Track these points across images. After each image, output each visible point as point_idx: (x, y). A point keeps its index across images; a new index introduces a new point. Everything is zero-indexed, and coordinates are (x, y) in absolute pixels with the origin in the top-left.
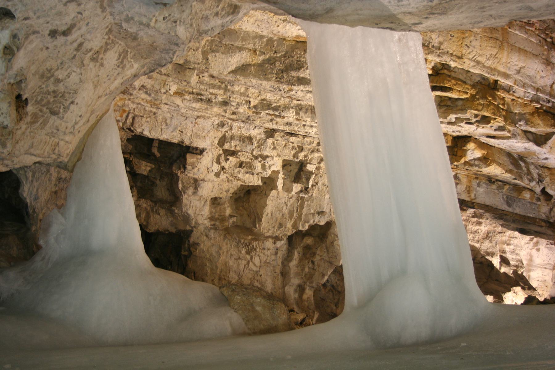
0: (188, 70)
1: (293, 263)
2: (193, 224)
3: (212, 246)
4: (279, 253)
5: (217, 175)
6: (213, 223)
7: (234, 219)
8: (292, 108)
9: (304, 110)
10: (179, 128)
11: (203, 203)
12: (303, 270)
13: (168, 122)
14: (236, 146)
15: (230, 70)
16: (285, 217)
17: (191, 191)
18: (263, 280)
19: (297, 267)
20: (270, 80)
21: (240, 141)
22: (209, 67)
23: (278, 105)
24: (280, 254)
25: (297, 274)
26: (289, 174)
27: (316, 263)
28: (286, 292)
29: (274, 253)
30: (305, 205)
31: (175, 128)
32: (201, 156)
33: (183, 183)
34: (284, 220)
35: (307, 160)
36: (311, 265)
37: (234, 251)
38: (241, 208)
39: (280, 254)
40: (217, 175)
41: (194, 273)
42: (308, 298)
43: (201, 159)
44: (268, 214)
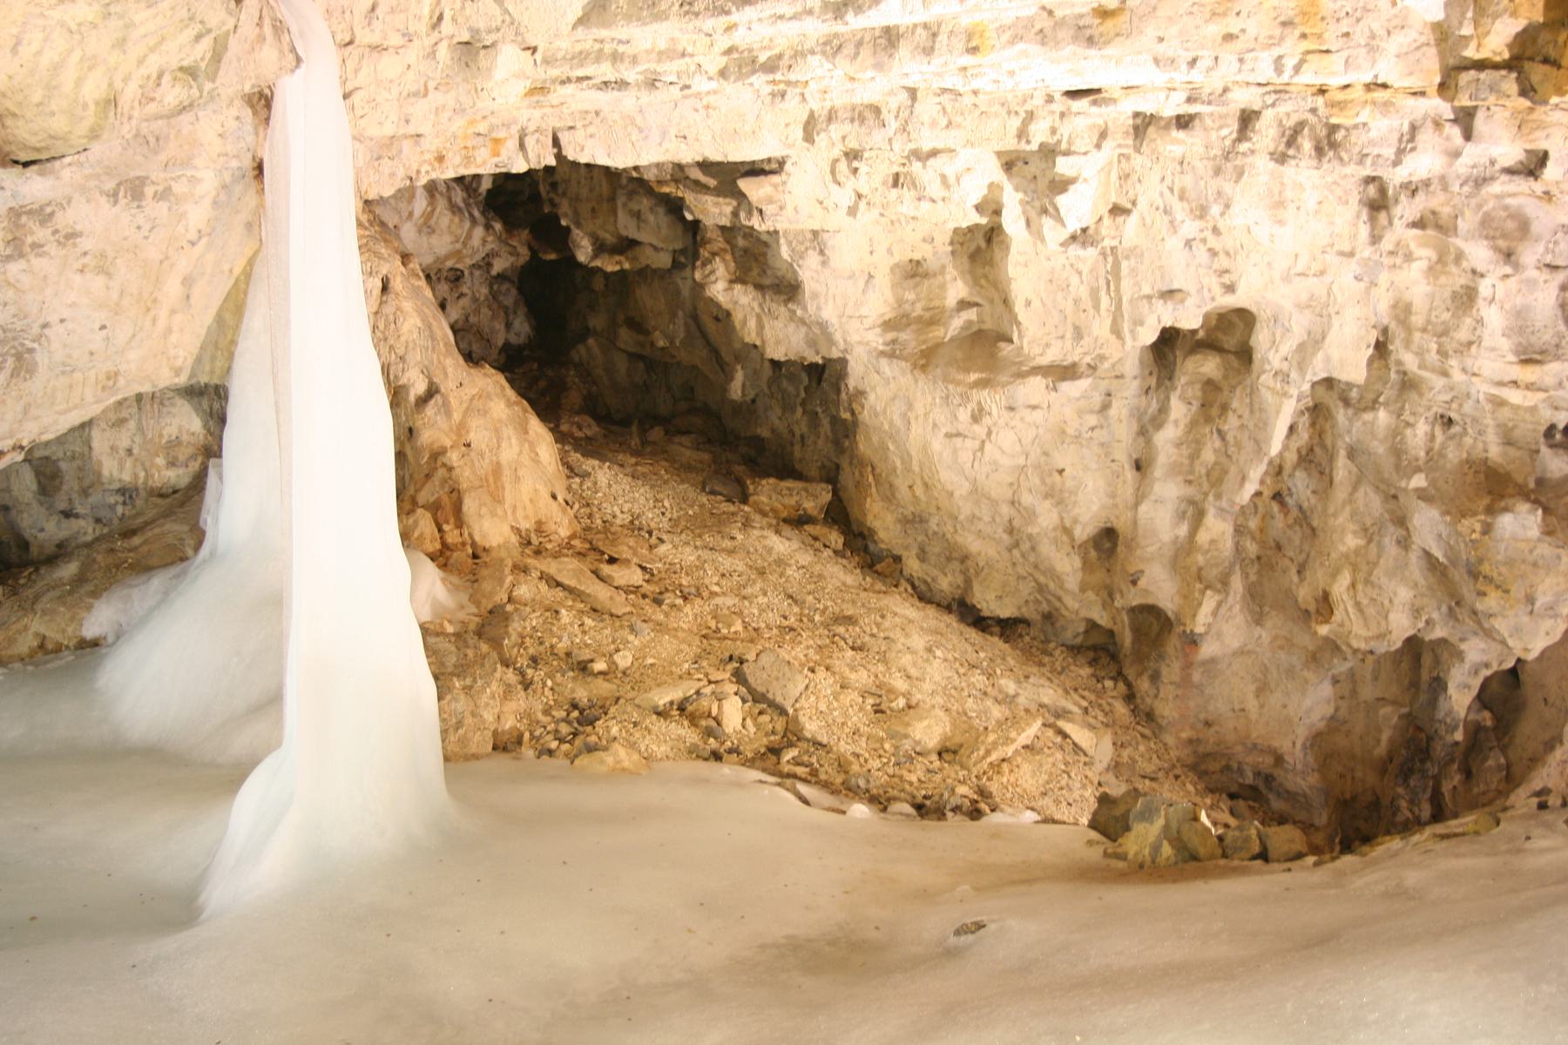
0: (482, 52)
1: (1166, 438)
2: (842, 345)
3: (893, 399)
4: (1115, 404)
5: (852, 211)
6: (891, 336)
7: (972, 314)
8: (813, 52)
9: (849, 49)
10: (673, 132)
11: (861, 283)
12: (1195, 456)
13: (639, 121)
14: (844, 138)
15: (572, 17)
16: (1082, 307)
17: (813, 260)
18: (1070, 484)
19: (1178, 445)
20: (667, 18)
21: (852, 121)
22: (522, 30)
23: (776, 51)
24: (1119, 409)
25: (1174, 469)
26: (1032, 186)
27: (1230, 437)
28: (1141, 522)
29: (1097, 407)
30: (1125, 271)
31: (664, 134)
32: (784, 176)
33: (789, 243)
34: (1083, 316)
35: (1059, 142)
36: (1218, 443)
37: (940, 415)
38: (983, 282)
39: (1119, 409)
40: (852, 211)
41: (873, 468)
42: (1213, 541)
43: (784, 183)
44: (1028, 303)
